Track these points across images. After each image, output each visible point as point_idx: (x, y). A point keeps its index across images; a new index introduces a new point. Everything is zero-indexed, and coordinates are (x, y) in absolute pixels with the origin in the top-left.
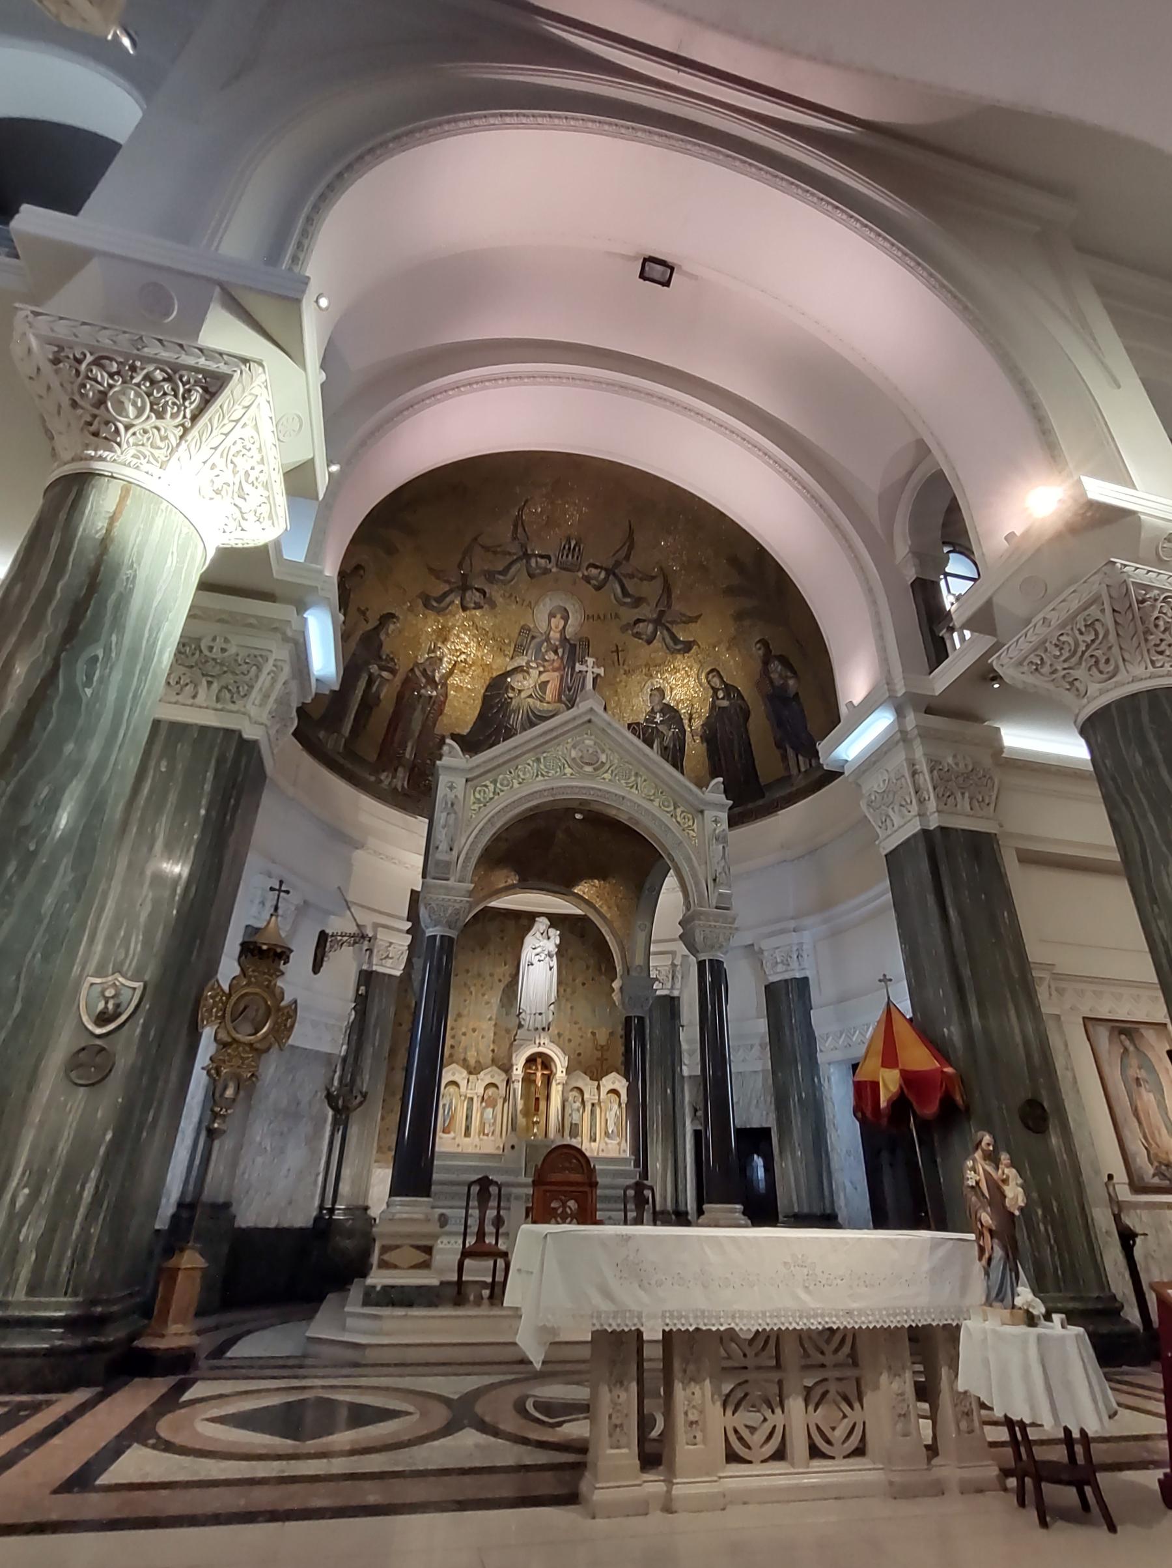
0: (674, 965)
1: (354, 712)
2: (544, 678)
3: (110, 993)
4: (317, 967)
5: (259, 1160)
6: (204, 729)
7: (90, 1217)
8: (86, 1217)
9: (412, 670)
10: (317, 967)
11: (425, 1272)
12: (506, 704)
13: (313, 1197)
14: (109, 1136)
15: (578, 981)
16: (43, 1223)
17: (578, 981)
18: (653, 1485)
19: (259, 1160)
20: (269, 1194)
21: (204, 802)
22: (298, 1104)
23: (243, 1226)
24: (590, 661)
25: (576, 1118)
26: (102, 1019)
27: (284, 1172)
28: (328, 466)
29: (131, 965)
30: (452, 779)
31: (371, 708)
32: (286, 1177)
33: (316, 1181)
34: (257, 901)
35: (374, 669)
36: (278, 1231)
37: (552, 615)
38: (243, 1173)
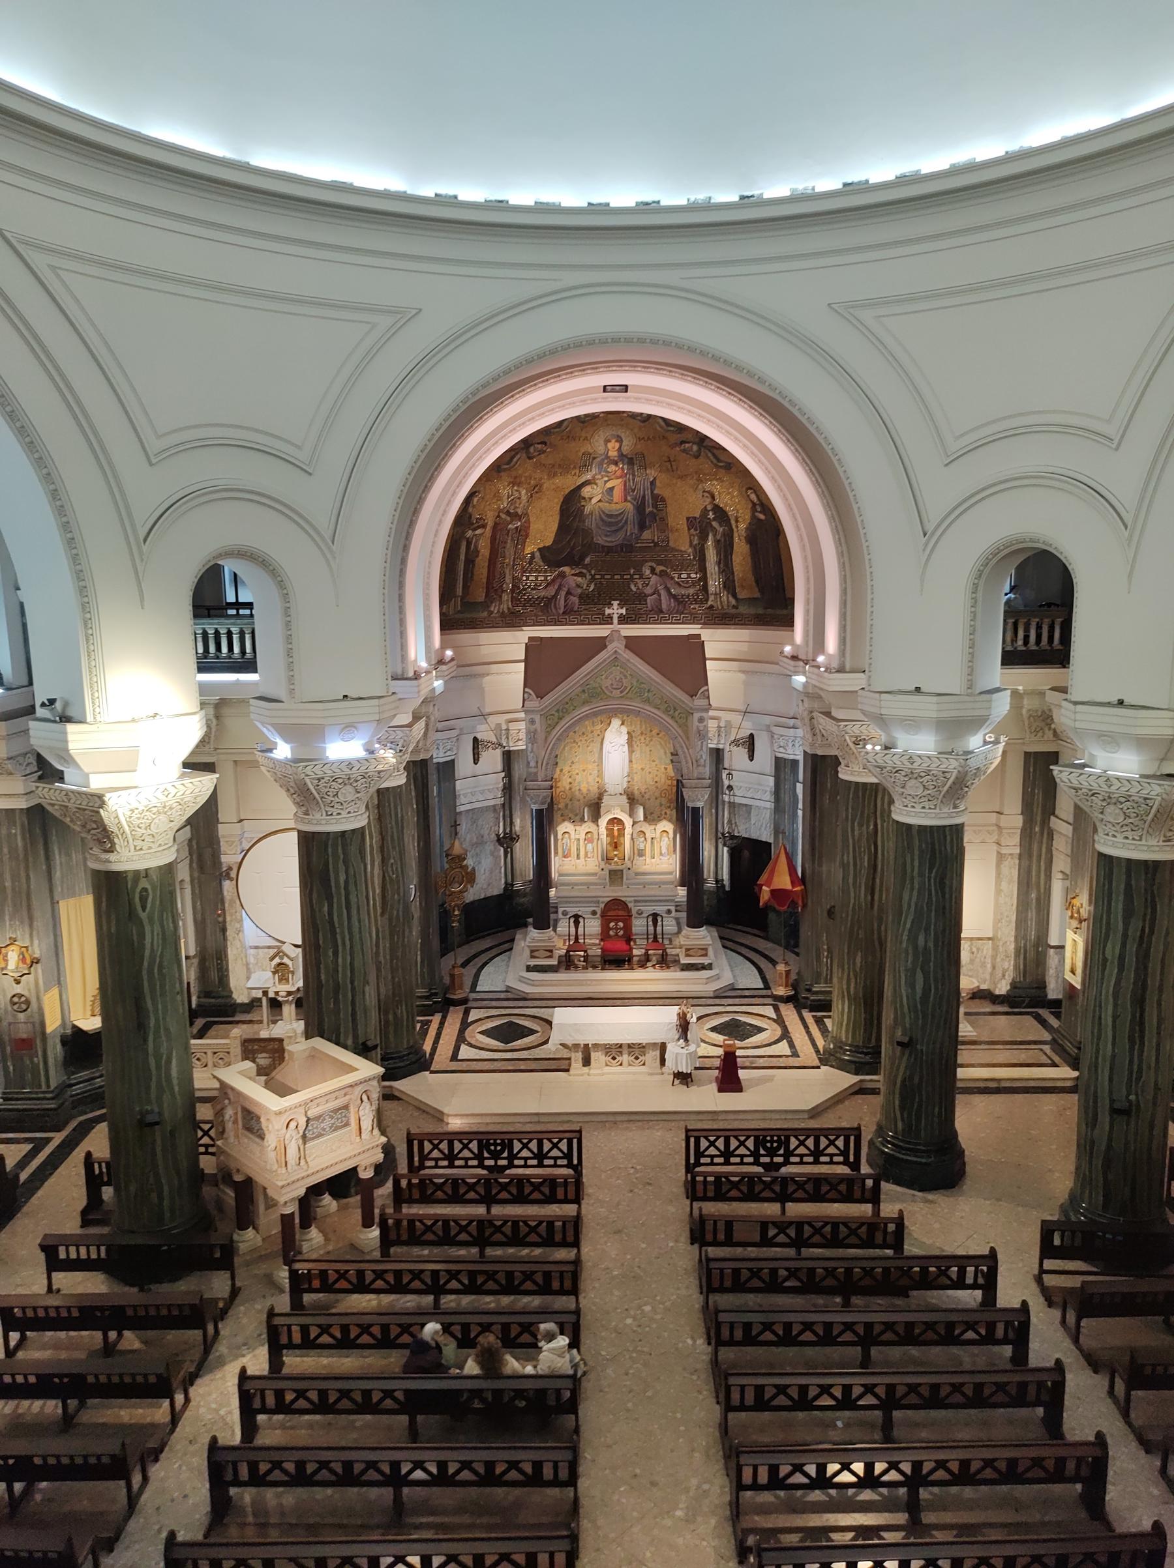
0: (719, 727)
2: (609, 485)
4: (476, 761)
9: (498, 516)
10: (476, 761)
12: (581, 509)
15: (654, 732)
17: (654, 732)
18: (586, 1069)
24: (615, 603)
25: (642, 847)
31: (473, 562)
35: (469, 533)
37: (607, 441)
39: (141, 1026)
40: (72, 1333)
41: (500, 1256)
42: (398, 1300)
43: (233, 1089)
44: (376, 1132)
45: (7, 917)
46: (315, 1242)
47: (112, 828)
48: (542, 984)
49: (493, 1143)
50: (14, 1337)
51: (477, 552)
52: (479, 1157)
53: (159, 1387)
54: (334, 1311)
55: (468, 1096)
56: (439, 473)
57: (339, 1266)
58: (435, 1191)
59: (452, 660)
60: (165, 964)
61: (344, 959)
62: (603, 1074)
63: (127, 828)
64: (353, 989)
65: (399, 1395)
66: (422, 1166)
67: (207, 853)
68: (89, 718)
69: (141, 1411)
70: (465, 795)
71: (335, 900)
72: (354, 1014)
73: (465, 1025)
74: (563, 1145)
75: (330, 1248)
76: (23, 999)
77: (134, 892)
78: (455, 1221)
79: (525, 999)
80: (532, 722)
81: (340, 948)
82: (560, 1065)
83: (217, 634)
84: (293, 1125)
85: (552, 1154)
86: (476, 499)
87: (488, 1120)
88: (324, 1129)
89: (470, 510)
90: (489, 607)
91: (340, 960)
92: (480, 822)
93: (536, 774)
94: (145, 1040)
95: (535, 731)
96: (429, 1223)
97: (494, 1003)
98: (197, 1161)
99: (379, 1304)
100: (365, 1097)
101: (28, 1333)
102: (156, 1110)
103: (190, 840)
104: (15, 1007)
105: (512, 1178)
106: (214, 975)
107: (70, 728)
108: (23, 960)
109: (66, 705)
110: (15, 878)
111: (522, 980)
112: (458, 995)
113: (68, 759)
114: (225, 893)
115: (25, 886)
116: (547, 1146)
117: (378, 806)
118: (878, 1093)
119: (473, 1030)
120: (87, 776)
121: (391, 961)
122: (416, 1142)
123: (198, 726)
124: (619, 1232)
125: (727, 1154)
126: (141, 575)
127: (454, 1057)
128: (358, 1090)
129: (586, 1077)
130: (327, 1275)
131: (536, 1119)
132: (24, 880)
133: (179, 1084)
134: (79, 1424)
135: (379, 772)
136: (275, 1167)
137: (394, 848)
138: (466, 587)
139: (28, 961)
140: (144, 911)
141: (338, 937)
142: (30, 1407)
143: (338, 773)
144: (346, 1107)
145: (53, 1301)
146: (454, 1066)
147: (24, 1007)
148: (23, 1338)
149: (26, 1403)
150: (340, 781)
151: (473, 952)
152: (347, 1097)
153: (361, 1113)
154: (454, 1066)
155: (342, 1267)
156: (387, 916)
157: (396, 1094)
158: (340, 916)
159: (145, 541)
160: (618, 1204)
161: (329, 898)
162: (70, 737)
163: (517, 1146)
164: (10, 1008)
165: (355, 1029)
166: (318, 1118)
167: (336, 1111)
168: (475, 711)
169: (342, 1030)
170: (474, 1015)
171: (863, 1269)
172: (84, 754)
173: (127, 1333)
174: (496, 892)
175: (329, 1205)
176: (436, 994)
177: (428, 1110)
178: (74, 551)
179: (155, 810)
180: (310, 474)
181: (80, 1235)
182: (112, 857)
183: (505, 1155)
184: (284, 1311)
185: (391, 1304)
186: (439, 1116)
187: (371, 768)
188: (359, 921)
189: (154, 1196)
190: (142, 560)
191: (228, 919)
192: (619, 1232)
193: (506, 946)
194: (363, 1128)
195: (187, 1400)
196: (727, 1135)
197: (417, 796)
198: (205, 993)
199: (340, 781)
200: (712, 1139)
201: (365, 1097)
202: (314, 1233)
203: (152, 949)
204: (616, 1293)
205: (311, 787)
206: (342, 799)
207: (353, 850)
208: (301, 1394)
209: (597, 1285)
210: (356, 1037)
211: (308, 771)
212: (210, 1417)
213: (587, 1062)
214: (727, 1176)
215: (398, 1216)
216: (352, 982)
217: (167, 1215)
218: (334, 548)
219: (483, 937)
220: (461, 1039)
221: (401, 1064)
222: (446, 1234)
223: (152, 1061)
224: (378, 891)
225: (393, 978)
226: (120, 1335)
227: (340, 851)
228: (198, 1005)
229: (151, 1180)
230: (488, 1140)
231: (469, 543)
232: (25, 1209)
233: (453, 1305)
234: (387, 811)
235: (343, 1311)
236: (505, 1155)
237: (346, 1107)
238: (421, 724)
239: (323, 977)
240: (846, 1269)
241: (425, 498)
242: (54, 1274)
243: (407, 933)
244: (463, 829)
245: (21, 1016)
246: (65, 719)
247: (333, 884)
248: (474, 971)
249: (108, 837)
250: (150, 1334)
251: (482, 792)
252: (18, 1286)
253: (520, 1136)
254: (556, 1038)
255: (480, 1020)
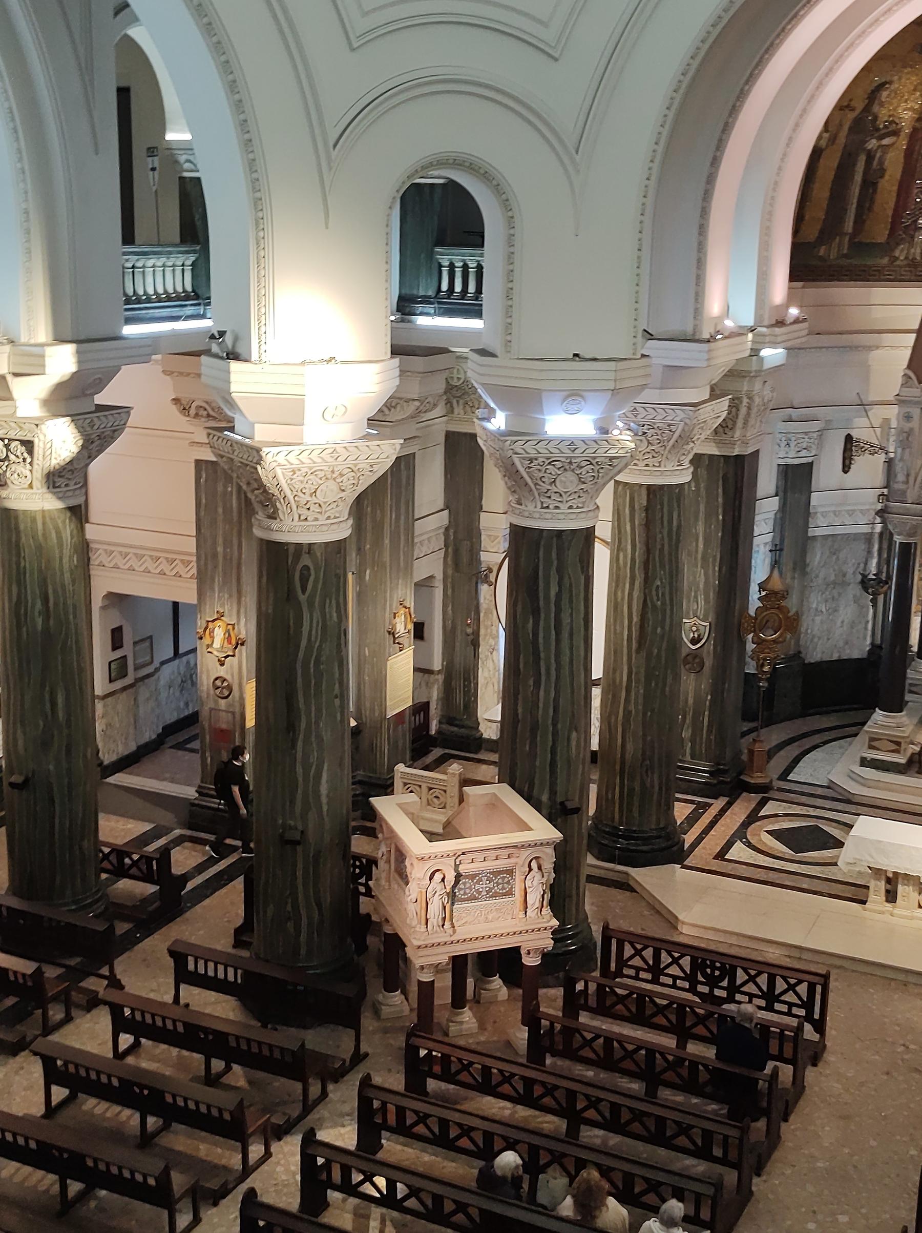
1: (855, 201)
3: (694, 629)
4: (846, 468)
5: (818, 619)
6: (711, 456)
7: (709, 731)
8: (707, 731)
10: (846, 468)
11: (896, 755)
13: (865, 638)
14: (709, 697)
16: (690, 731)
19: (818, 619)
20: (828, 639)
21: (720, 510)
22: (844, 575)
23: (813, 661)
26: (694, 641)
27: (839, 624)
28: (690, 1061)
29: (700, 613)
30: (908, 410)
31: (875, 185)
32: (842, 627)
33: (866, 629)
34: (783, 444)
35: (872, 144)
36: (840, 661)
38: (807, 630)
39: (291, 728)
40: (185, 1053)
41: (679, 1103)
42: (535, 1117)
43: (387, 824)
44: (547, 911)
45: (216, 589)
46: (465, 1026)
47: (274, 490)
48: (877, 785)
49: (714, 967)
50: (126, 1040)
51: (882, 171)
52: (691, 978)
53: (233, 1129)
54: (458, 1107)
55: (710, 901)
56: (772, 55)
57: (590, 1091)
58: (616, 1004)
59: (797, 321)
60: (323, 659)
61: (547, 692)
62: (912, 918)
63: (288, 493)
64: (555, 734)
65: (474, 1212)
66: (619, 973)
67: (466, 545)
68: (254, 357)
69: (219, 1150)
70: (824, 514)
71: (543, 616)
72: (553, 764)
73: (753, 818)
74: (803, 989)
75: (482, 1039)
76: (225, 684)
77: (294, 569)
78: (703, 1065)
79: (849, 802)
80: (908, 417)
81: (543, 678)
82: (856, 893)
83: (465, 267)
84: (438, 877)
85: (786, 998)
86: (885, 94)
87: (733, 940)
88: (480, 893)
89: (875, 108)
90: (893, 250)
91: (542, 693)
92: (842, 556)
93: (904, 493)
94: (294, 746)
95: (910, 433)
96: (630, 1047)
97: (804, 799)
98: (357, 904)
99: (512, 1115)
100: (534, 865)
101: (143, 1040)
102: (300, 828)
103: (447, 529)
104: (218, 691)
105: (632, 990)
106: (459, 699)
107: (234, 365)
108: (229, 639)
109: (236, 339)
110: (227, 543)
111: (853, 776)
112: (756, 779)
113: (231, 404)
114: (482, 600)
115: (236, 553)
116: (780, 985)
117: (647, 509)
118: (588, 876)
119: (761, 827)
120: (252, 425)
121: (645, 714)
122: (614, 942)
123: (377, 378)
124: (846, 1118)
125: (656, 971)
126: (327, 189)
127: (721, 855)
128: (526, 854)
129: (887, 917)
130: (450, 1062)
131: (796, 954)
132: (235, 548)
133: (328, 803)
134: (156, 1145)
135: (611, 459)
136: (415, 923)
137: (662, 566)
138: (859, 221)
139: (234, 642)
140: (304, 591)
141: (542, 663)
142: (120, 1113)
143: (556, 455)
144: (510, 872)
145: (177, 1013)
146: (716, 865)
147: (226, 693)
148: (136, 1045)
149: (104, 1105)
150: (559, 464)
151: (805, 729)
152: (512, 860)
153: (528, 883)
154: (716, 865)
155: (467, 1057)
156: (644, 654)
157: (631, 883)
158: (547, 638)
159: (335, 146)
160: (862, 1084)
161: (536, 612)
162: (233, 378)
163: (741, 976)
164: (212, 692)
165: (553, 785)
166: (472, 877)
167: (496, 873)
168: (852, 398)
169: (537, 782)
170: (770, 808)
171: (501, 1071)
172: (247, 398)
173: (236, 1067)
174: (856, 655)
175: (499, 990)
176: (725, 772)
177: (663, 912)
178: (251, 156)
179: (321, 474)
180: (556, 60)
181: (229, 954)
182: (275, 525)
183: (725, 983)
184: (395, 1088)
185: (525, 1119)
186: (672, 922)
187: (601, 452)
188: (571, 649)
189: (290, 925)
190: (330, 169)
191: (482, 632)
192: (846, 1118)
193: (850, 730)
194: (530, 901)
195: (268, 1154)
196: (773, 971)
197: (725, 504)
198: (448, 719)
199: (559, 464)
200: (792, 981)
201: (534, 865)
202: (467, 1016)
203: (309, 640)
204: (810, 1188)
205: (522, 470)
206: (561, 489)
207: (572, 556)
208: (413, 1192)
209: (788, 1172)
210: (553, 793)
211: (518, 447)
212: (284, 1177)
213: (891, 896)
214: (651, 994)
215: (680, 1053)
216: (554, 725)
217: (303, 951)
218: (578, 158)
219: (827, 713)
220: (740, 834)
221: (645, 848)
222: (611, 1056)
223: (299, 770)
224: (635, 619)
225: (644, 735)
226: (228, 1068)
227: (554, 555)
228: (439, 732)
229: (289, 908)
230: (704, 960)
231: (870, 156)
232: (188, 915)
233: (598, 1141)
234: (658, 516)
235: (470, 1110)
236: (725, 983)
237: (510, 872)
238: (723, 405)
239: (520, 710)
240: (484, 1067)
241: (749, 91)
242: (183, 987)
243: (669, 680)
244: (816, 557)
245: (223, 702)
246: (233, 356)
247: (541, 595)
248: (797, 753)
249: (269, 500)
250: (260, 1075)
251: (851, 513)
252: (152, 991)
253: (746, 964)
254: (845, 856)
255: (776, 816)
